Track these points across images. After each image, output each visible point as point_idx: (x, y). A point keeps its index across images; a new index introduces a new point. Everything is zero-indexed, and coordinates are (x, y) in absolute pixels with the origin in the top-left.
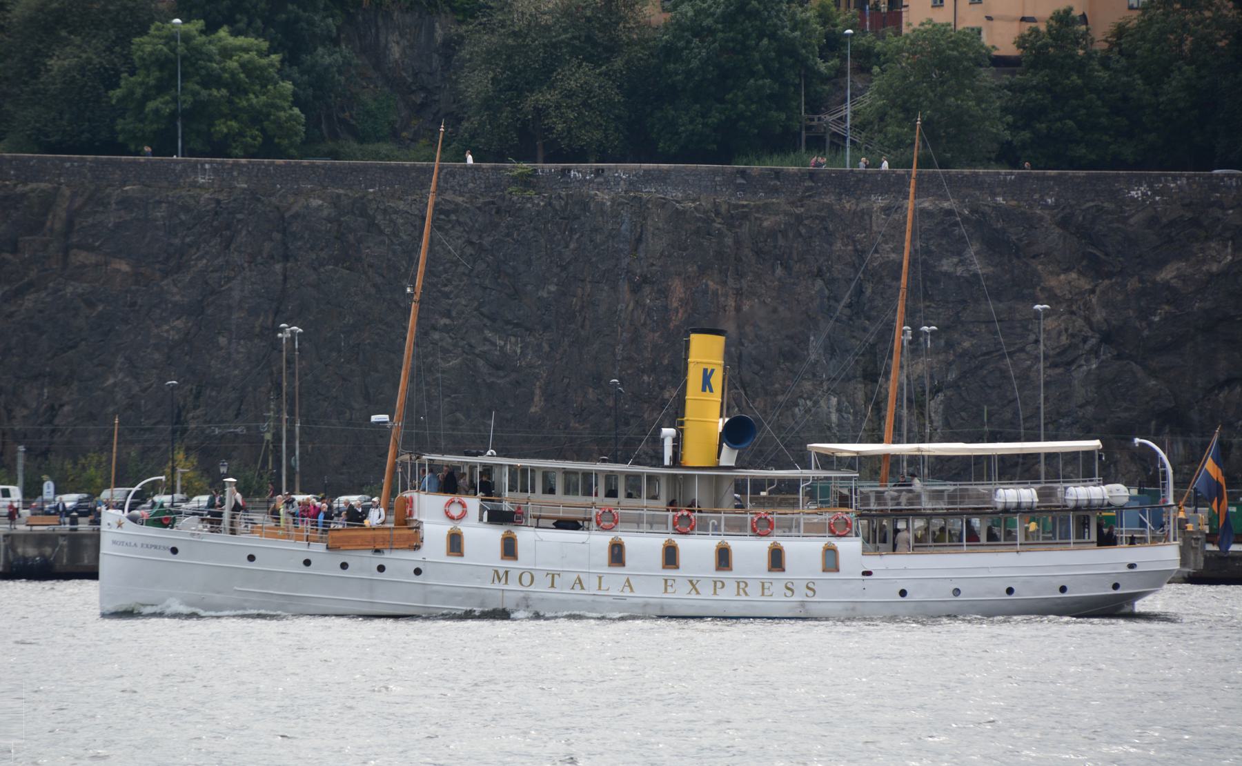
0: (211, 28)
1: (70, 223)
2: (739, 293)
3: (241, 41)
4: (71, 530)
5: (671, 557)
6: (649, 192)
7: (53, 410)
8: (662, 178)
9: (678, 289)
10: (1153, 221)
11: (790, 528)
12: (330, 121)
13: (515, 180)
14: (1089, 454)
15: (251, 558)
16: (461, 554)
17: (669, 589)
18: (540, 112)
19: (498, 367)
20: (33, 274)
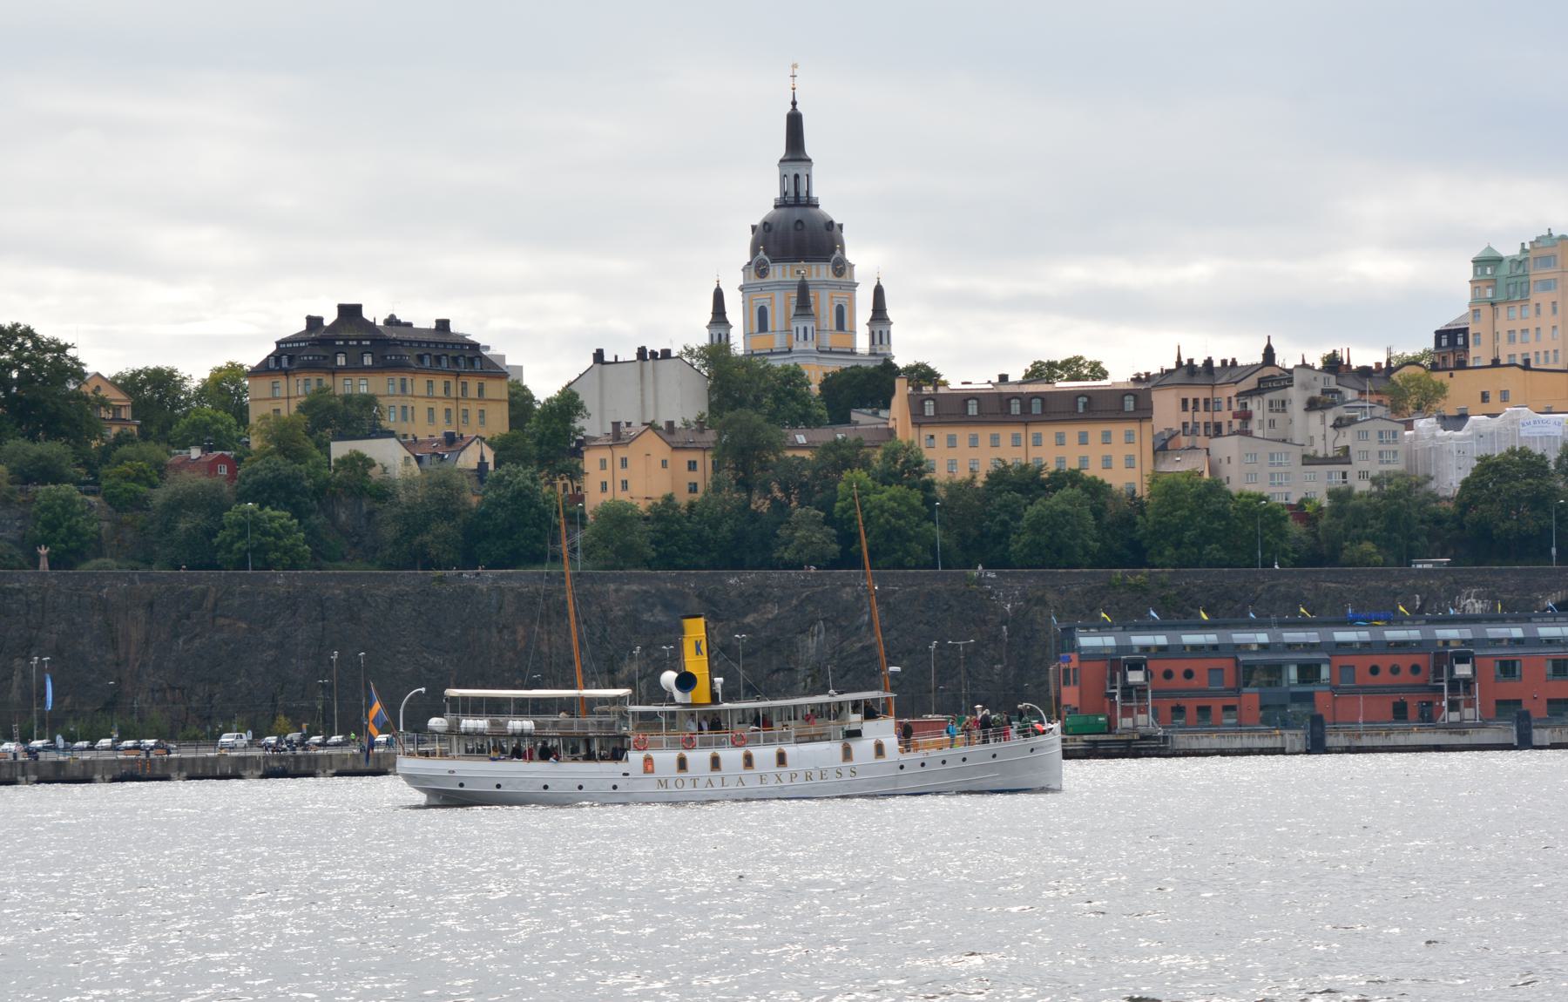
0: (261, 508)
1: (216, 604)
2: (549, 633)
3: (276, 513)
5: (682, 764)
6: (503, 583)
7: (211, 696)
8: (510, 576)
9: (521, 631)
10: (741, 594)
11: (658, 746)
12: (322, 555)
13: (435, 579)
14: (45, 703)
18: (423, 545)
19: (430, 671)
20: (198, 630)
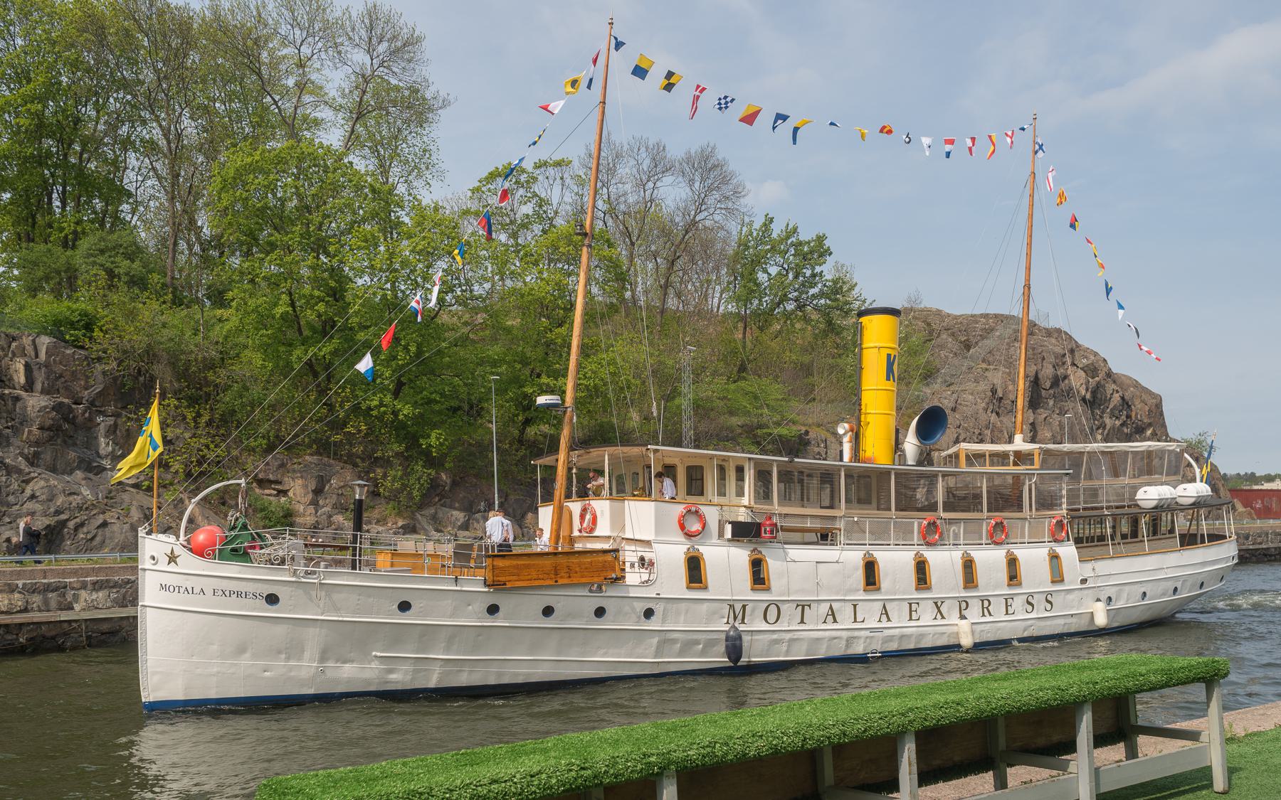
4: (1202, 536)
15: (404, 607)
16: (929, 588)
17: (914, 616)
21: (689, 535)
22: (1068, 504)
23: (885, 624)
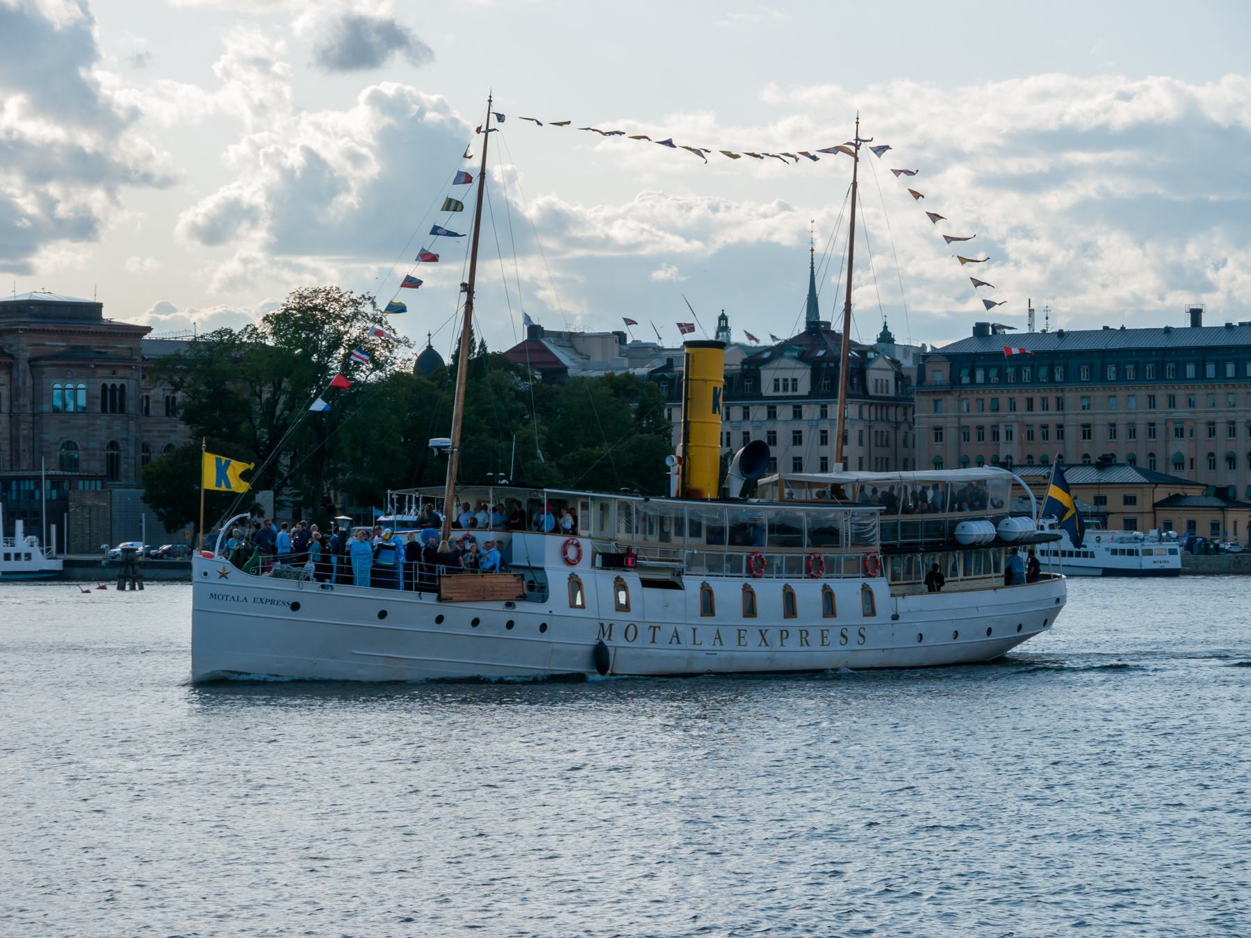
21: (568, 562)
22: (881, 539)
23: (718, 647)
